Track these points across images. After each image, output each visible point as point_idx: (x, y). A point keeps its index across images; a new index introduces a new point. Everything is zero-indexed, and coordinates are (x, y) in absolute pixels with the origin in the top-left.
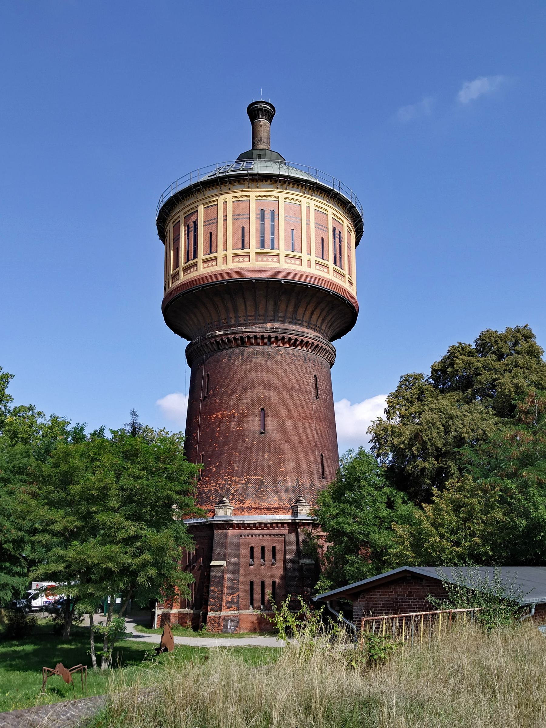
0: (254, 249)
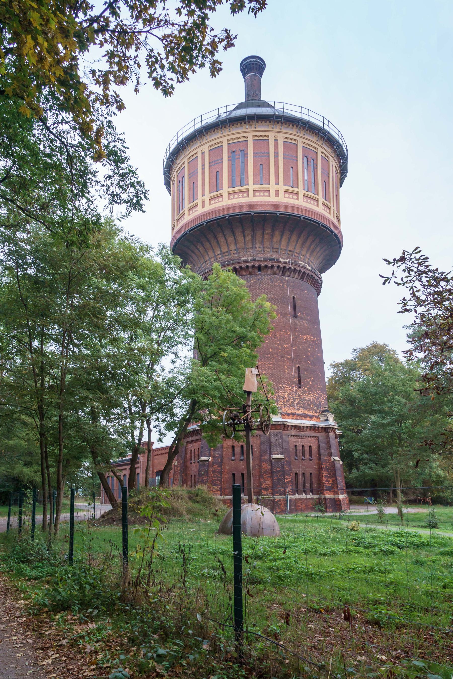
0: (226, 190)
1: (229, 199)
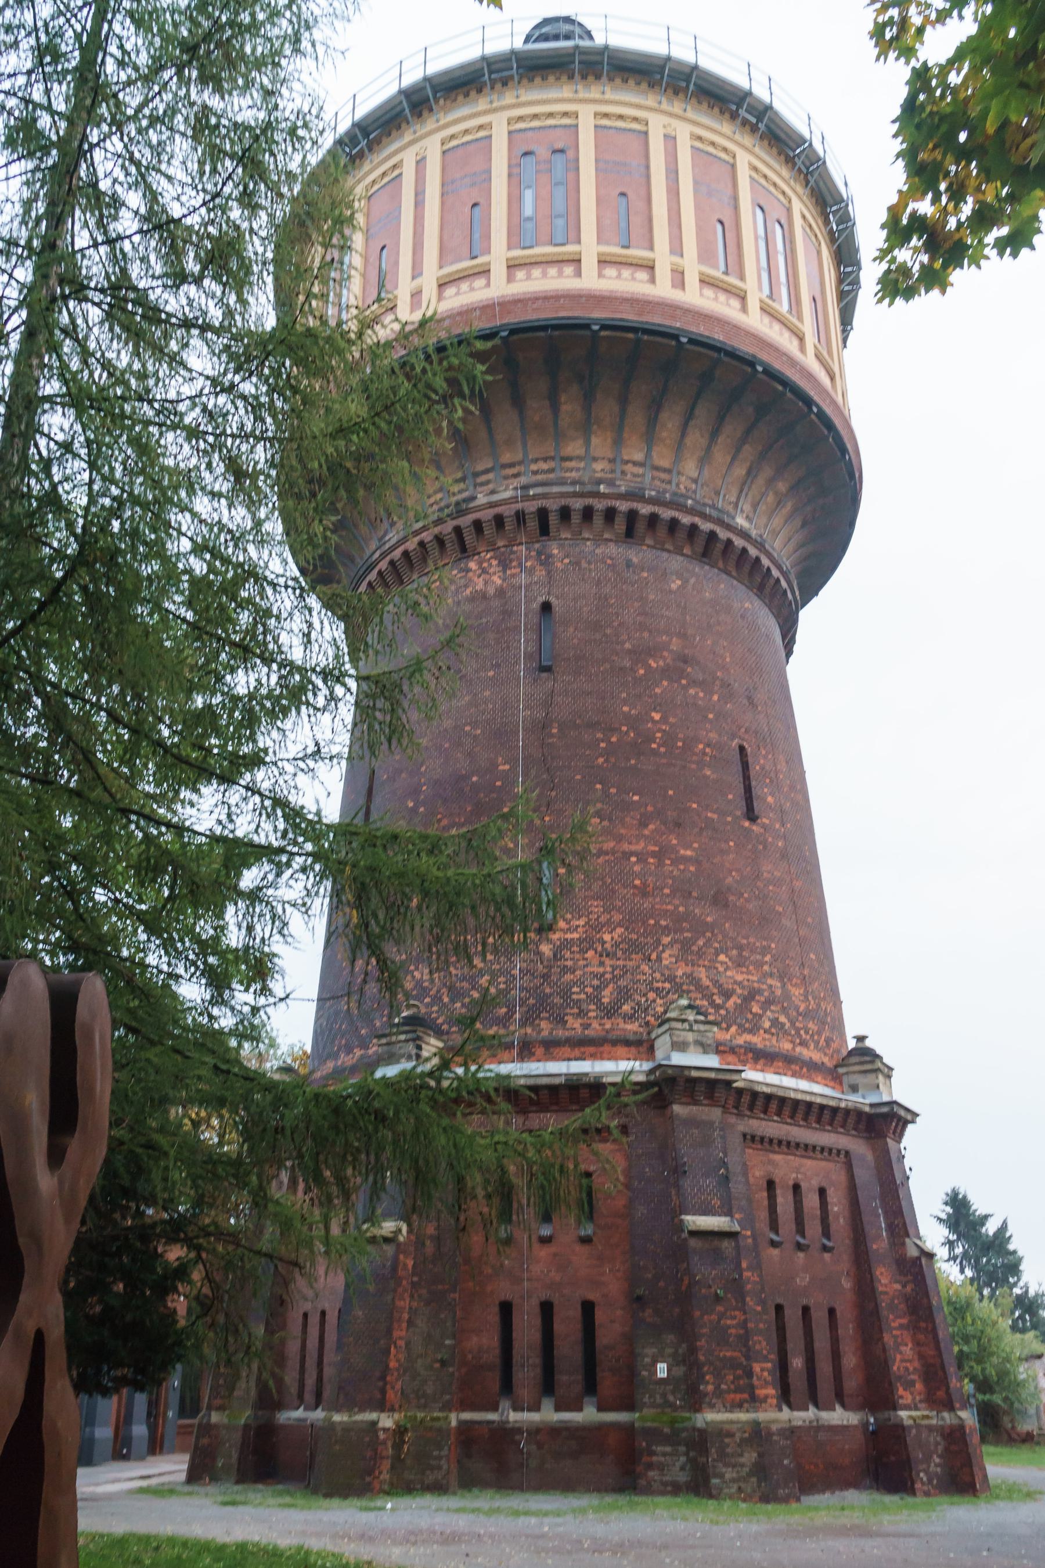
1: (510, 279)
